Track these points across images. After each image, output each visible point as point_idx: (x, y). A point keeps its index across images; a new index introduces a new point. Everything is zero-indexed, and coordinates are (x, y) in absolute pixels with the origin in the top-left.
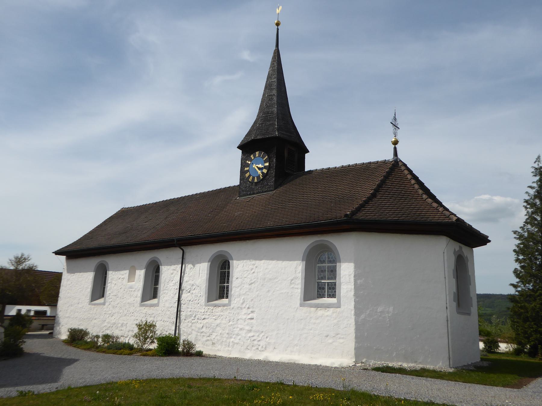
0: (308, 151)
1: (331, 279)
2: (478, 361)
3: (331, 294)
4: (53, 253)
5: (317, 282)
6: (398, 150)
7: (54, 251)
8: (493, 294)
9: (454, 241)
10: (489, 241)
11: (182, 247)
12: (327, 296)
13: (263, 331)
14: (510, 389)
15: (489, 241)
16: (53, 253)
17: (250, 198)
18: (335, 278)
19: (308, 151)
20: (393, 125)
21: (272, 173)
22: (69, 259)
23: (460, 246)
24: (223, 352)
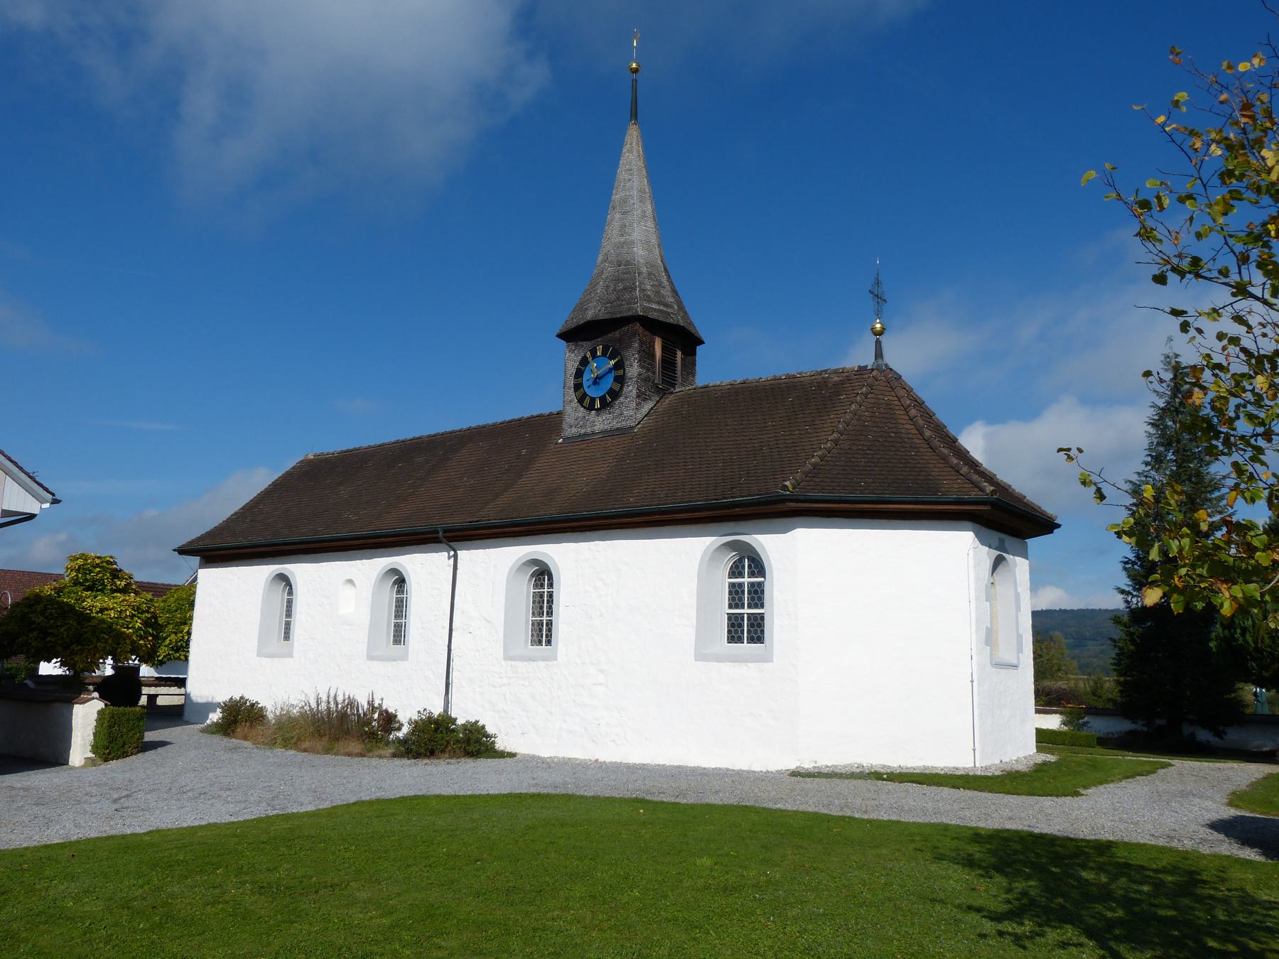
0: (701, 342)
1: (756, 606)
2: (1032, 754)
3: (736, 628)
4: (174, 550)
5: (728, 614)
6: (884, 345)
7: (176, 547)
8: (1048, 729)
9: (987, 530)
10: (1058, 526)
11: (451, 544)
12: (747, 640)
13: (1150, 835)
14: (491, 760)
15: (1058, 526)
16: (174, 550)
17: (588, 441)
18: (762, 606)
19: (701, 342)
20: (876, 295)
21: (631, 391)
22: (209, 563)
23: (999, 539)
24: (546, 750)
